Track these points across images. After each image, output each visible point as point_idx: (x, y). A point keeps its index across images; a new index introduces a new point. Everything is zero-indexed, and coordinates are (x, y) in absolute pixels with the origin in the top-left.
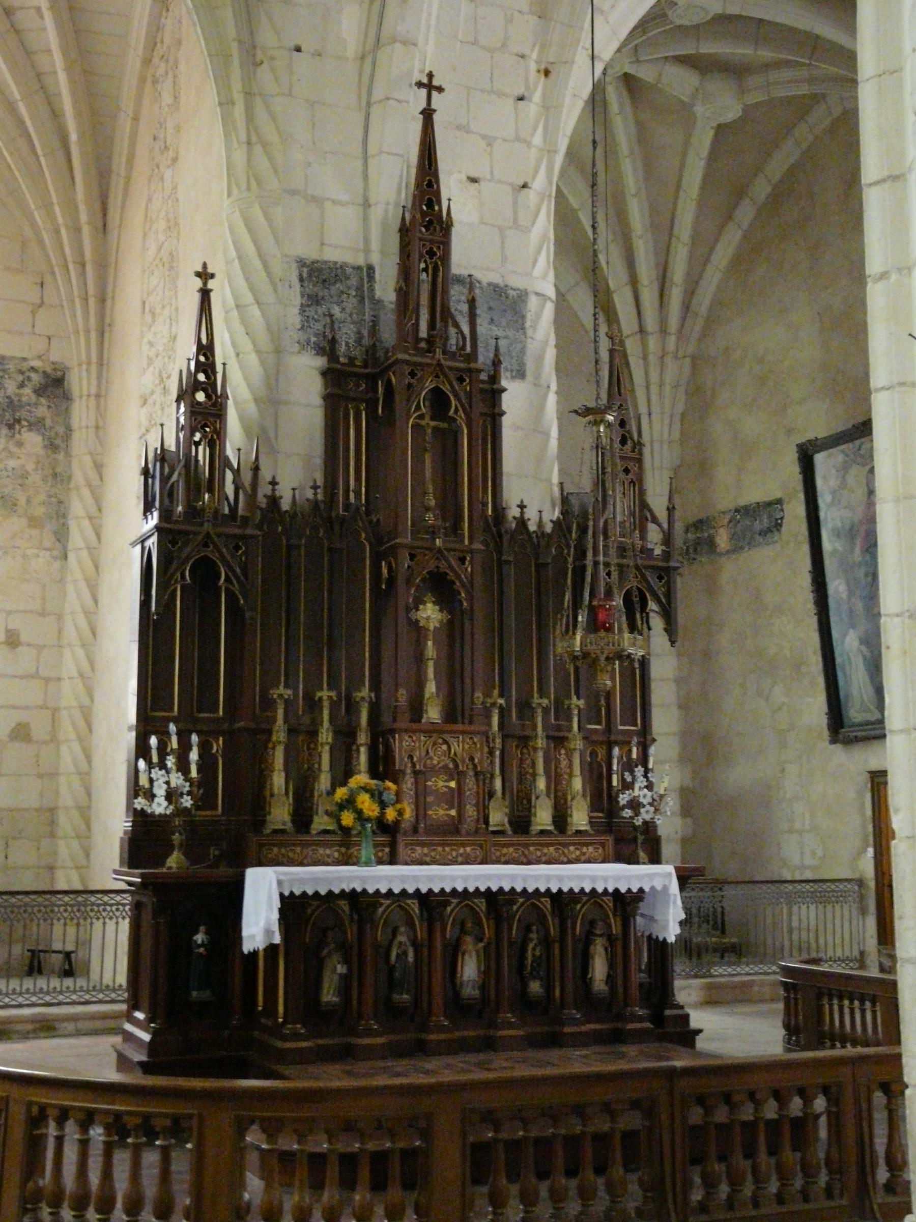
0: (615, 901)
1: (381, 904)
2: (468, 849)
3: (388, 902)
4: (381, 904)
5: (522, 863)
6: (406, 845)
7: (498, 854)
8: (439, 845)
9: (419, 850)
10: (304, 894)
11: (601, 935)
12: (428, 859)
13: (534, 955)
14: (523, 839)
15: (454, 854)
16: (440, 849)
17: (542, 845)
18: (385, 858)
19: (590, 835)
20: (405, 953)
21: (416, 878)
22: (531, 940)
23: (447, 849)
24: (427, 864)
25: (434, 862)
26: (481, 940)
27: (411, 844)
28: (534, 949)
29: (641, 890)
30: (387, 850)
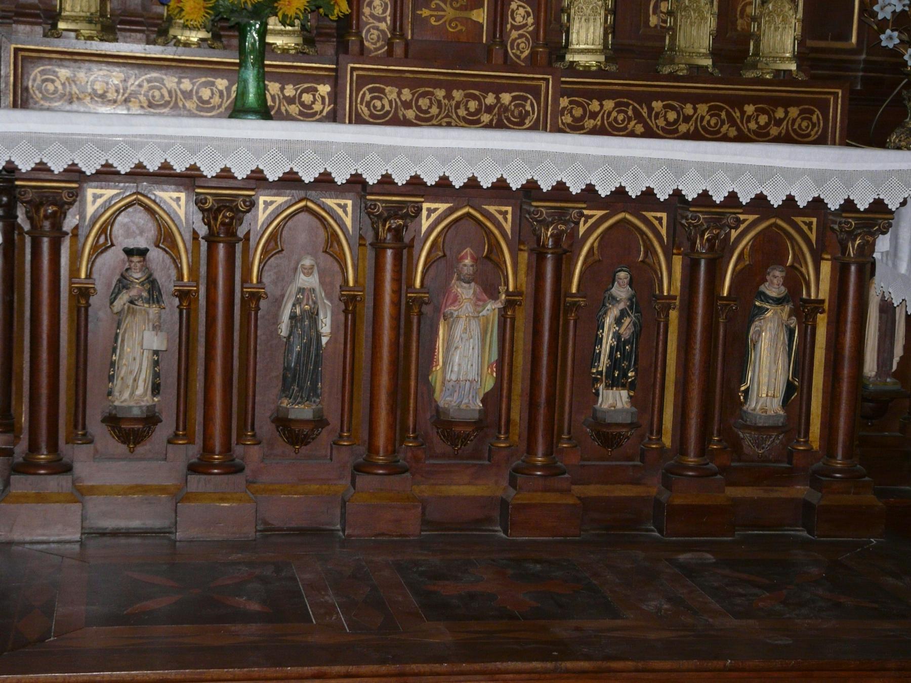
0: (365, 210)
1: (739, 222)
2: (506, 98)
3: (751, 218)
4: (739, 222)
5: (725, 139)
6: (362, 81)
7: (578, 112)
8: (438, 84)
9: (391, 92)
10: (840, 205)
11: (779, 301)
12: (410, 114)
13: (617, 336)
14: (639, 85)
15: (473, 105)
16: (440, 93)
17: (685, 98)
18: (317, 107)
19: (711, 79)
20: (313, 316)
21: (415, 155)
22: (614, 299)
23: (458, 95)
24: (407, 123)
25: (424, 120)
26: (494, 296)
27: (374, 80)
28: (618, 321)
29: (878, 205)
30: (324, 89)
